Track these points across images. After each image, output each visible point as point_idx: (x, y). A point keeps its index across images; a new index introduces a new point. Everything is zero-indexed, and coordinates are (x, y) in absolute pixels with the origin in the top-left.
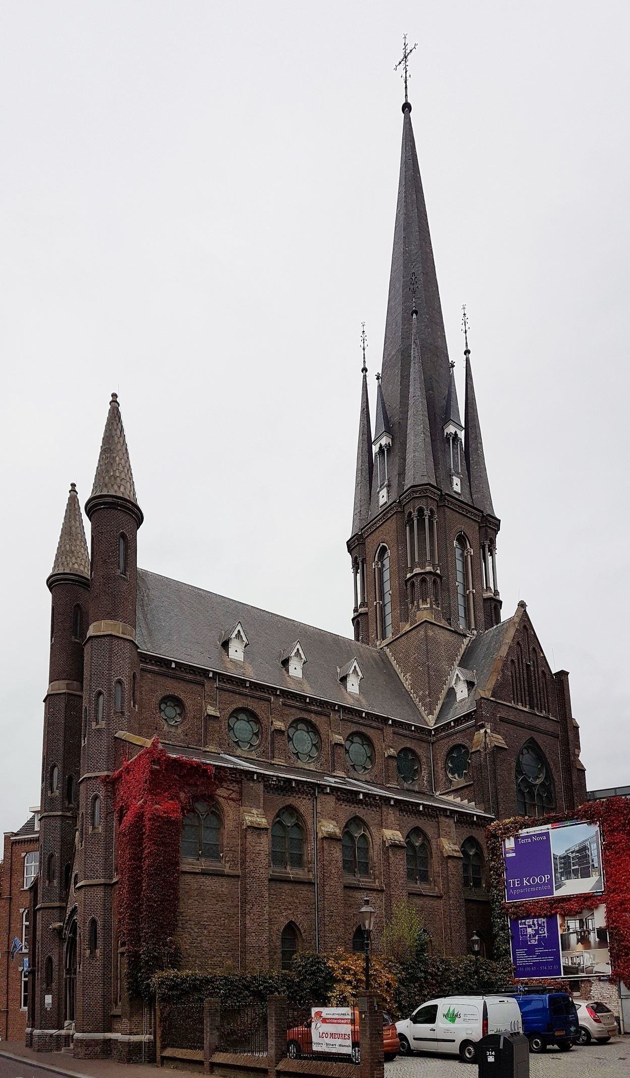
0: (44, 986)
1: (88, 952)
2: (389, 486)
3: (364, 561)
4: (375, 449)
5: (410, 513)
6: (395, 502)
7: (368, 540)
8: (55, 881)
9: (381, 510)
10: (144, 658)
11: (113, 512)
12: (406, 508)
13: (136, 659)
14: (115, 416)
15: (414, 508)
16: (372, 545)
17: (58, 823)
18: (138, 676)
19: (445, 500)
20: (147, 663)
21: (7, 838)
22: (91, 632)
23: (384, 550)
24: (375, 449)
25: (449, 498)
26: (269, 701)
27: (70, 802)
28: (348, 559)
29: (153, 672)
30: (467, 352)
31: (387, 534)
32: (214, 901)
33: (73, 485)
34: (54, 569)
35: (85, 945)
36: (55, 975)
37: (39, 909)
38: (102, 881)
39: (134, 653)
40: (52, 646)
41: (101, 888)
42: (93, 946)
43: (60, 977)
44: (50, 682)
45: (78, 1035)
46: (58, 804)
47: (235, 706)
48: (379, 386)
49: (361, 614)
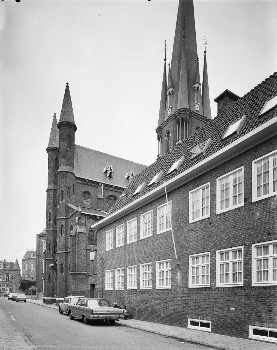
0: (48, 284)
1: (60, 273)
2: (172, 108)
3: (161, 137)
5: (178, 120)
6: (173, 115)
8: (51, 251)
9: (168, 118)
10: (77, 178)
11: (66, 127)
12: (177, 117)
14: (67, 87)
16: (165, 130)
17: (51, 232)
18: (75, 185)
19: (192, 114)
21: (37, 235)
22: (59, 170)
23: (169, 133)
28: (156, 136)
30: (205, 52)
31: (170, 127)
33: (67, 84)
36: (52, 280)
37: (46, 259)
39: (74, 177)
40: (48, 172)
41: (64, 254)
42: (61, 272)
43: (53, 281)
46: (51, 226)
47: (108, 195)
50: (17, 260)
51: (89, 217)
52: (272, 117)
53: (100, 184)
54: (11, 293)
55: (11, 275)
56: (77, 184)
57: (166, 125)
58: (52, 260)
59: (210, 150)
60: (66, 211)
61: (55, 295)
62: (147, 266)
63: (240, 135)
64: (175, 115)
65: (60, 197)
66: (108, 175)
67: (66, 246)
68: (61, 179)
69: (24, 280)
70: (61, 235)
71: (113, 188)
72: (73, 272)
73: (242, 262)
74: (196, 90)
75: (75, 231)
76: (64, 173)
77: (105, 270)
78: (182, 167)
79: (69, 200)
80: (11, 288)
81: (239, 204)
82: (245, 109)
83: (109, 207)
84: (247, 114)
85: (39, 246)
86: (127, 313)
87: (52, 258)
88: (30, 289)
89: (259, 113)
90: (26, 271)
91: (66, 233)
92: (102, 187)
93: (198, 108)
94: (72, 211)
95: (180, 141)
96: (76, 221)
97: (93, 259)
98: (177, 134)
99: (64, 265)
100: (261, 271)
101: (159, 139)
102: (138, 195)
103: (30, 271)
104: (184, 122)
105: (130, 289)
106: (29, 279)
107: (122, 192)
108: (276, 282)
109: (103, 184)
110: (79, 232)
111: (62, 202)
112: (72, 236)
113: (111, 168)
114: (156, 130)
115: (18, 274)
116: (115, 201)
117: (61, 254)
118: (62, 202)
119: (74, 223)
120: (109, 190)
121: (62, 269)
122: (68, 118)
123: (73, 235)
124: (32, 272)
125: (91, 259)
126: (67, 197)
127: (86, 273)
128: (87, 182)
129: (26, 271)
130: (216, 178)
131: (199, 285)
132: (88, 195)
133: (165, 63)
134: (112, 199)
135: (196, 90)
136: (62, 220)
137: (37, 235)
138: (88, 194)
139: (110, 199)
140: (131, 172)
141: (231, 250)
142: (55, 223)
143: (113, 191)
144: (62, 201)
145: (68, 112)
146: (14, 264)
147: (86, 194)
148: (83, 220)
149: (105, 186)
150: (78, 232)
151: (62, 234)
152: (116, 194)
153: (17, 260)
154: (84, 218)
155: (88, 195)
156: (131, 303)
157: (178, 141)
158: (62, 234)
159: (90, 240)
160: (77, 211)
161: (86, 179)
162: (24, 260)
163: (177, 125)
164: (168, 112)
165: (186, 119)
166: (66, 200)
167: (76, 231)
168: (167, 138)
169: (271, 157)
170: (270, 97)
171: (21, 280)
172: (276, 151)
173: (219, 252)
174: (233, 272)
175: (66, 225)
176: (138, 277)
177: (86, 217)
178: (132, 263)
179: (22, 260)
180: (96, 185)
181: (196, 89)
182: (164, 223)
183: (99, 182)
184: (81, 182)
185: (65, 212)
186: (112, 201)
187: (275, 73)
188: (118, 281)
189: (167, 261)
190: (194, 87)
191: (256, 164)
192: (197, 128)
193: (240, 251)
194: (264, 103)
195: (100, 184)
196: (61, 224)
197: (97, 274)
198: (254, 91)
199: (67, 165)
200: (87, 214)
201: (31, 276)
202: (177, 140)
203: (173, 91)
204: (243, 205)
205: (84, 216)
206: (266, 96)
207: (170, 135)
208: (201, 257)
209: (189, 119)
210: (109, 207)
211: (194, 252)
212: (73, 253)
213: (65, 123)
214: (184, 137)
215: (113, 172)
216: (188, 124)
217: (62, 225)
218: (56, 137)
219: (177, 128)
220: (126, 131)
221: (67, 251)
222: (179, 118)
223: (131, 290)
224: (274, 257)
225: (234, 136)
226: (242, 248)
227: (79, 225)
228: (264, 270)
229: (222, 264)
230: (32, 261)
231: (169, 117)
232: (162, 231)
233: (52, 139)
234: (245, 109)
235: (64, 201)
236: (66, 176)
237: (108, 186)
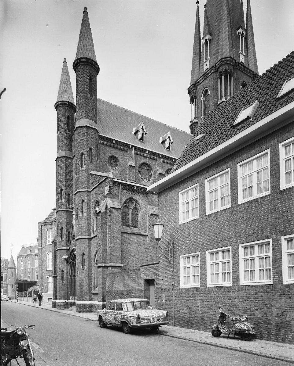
0: (61, 282)
1: (81, 267)
3: (196, 98)
4: (203, 42)
5: (221, 72)
6: (213, 67)
7: (198, 87)
9: (204, 72)
10: (101, 138)
13: (98, 138)
14: (85, 12)
15: (223, 69)
16: (201, 88)
17: (64, 213)
20: (102, 140)
23: (207, 91)
24: (203, 42)
25: (239, 65)
26: (156, 160)
27: (69, 205)
28: (188, 98)
29: (105, 145)
31: (209, 83)
32: (137, 246)
33: (86, 8)
34: (58, 99)
35: (80, 264)
37: (58, 250)
38: (87, 237)
39: (97, 135)
41: (87, 240)
42: (83, 265)
43: (67, 278)
44: (58, 151)
45: (77, 302)
46: (64, 205)
47: (141, 162)
48: (205, 11)
49: (194, 123)
50: (12, 257)
51: (123, 187)
52: (287, 103)
53: (131, 147)
54: (5, 295)
55: (5, 275)
56: (101, 145)
57: (203, 81)
58: (66, 251)
59: (223, 136)
60: (88, 181)
61: (71, 297)
62: (191, 258)
63: (253, 122)
64: (215, 67)
65: (80, 162)
66: (140, 136)
67: (89, 229)
68: (79, 138)
69: (21, 280)
70: (81, 213)
71: (146, 153)
72: (103, 265)
73: (230, 262)
74: (240, 37)
75: (105, 206)
76: (84, 129)
77: (178, 255)
78: (257, 116)
79: (92, 166)
80: (6, 289)
81: (250, 198)
82: (244, 100)
83: (142, 179)
84: (259, 100)
85: (41, 238)
86: (253, 328)
87: (65, 248)
88: (29, 290)
89: (277, 95)
90: (22, 269)
91: (88, 211)
92: (134, 152)
93: (242, 59)
94: (98, 180)
95: (224, 100)
96: (106, 192)
97: (160, 237)
98: (218, 92)
99: (86, 254)
100: (263, 270)
101: (192, 101)
102: (248, 122)
103: (26, 270)
104: (228, 75)
105: (251, 284)
106: (25, 279)
107: (158, 159)
108: (293, 279)
109: (135, 147)
110: (111, 207)
111: (83, 169)
112: (100, 214)
113: (142, 127)
114: (188, 89)
115: (14, 273)
116: (148, 171)
117: (82, 240)
118: (83, 169)
119: (101, 195)
120: (142, 156)
121: (84, 261)
122: (89, 54)
123: (102, 211)
124: (29, 270)
125: (156, 237)
126: (89, 162)
127: (121, 265)
128: (114, 143)
129: (22, 269)
130: (205, 179)
131: (189, 285)
132: (115, 162)
133: (198, 7)
134: (145, 168)
135: (240, 37)
136: (82, 193)
137: (39, 223)
138: (115, 160)
139: (142, 169)
140: (167, 135)
141: (256, 244)
142: (68, 201)
143: (146, 157)
144: (82, 167)
145: (88, 46)
146: (8, 262)
147: (112, 160)
148: (116, 191)
149: (137, 150)
150: (109, 207)
151: (82, 212)
152: (150, 162)
153: (12, 257)
154: (116, 188)
155: (115, 161)
156: (256, 309)
157: (221, 99)
158: (82, 212)
159: (124, 219)
160: (108, 177)
161: (113, 140)
162: (19, 257)
163: (219, 79)
164: (205, 66)
165: (231, 71)
166: (88, 166)
167: (107, 206)
168: (204, 98)
169: (254, 160)
170: (288, 78)
171: (17, 280)
172: (293, 138)
173: (285, 239)
174: (259, 268)
175: (89, 200)
176: (236, 265)
177: (119, 187)
178: (222, 242)
179: (17, 257)
180: (125, 148)
181: (240, 35)
182: (217, 199)
183: (130, 145)
184: (106, 143)
185: (86, 182)
186: (146, 171)
187: (292, 53)
188: (260, 267)
189: (188, 256)
190: (237, 33)
191: (241, 167)
192: (244, 85)
193: (267, 244)
194: (282, 85)
195: (131, 147)
196: (81, 199)
197: (158, 263)
198: (274, 68)
199: (88, 118)
200: (121, 183)
201: (28, 275)
202: (219, 98)
203: (211, 38)
204: (270, 193)
205: (117, 185)
206: (279, 81)
207: (209, 93)
208: (258, 246)
209: (234, 71)
210: (142, 179)
211: (195, 251)
212: (103, 238)
213: (84, 60)
214: (229, 94)
215: (146, 133)
216: (232, 77)
217: (83, 201)
218: (68, 88)
219: (218, 84)
220: (154, 89)
221: (90, 235)
222: (222, 70)
223: (253, 286)
224: (222, 262)
225: (246, 122)
226: (230, 249)
227: (111, 198)
228: (251, 269)
229: (247, 260)
230: (29, 258)
231: (207, 71)
232: (263, 193)
233: (62, 91)
234: (244, 100)
235: (84, 168)
236: (87, 133)
237: (140, 150)
